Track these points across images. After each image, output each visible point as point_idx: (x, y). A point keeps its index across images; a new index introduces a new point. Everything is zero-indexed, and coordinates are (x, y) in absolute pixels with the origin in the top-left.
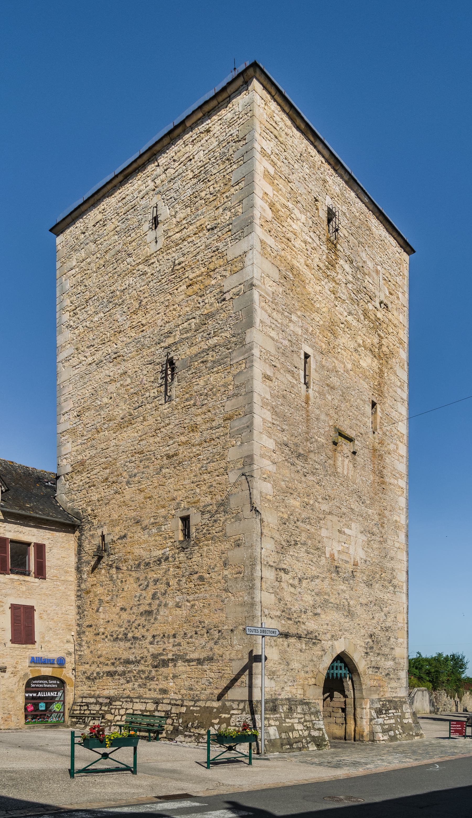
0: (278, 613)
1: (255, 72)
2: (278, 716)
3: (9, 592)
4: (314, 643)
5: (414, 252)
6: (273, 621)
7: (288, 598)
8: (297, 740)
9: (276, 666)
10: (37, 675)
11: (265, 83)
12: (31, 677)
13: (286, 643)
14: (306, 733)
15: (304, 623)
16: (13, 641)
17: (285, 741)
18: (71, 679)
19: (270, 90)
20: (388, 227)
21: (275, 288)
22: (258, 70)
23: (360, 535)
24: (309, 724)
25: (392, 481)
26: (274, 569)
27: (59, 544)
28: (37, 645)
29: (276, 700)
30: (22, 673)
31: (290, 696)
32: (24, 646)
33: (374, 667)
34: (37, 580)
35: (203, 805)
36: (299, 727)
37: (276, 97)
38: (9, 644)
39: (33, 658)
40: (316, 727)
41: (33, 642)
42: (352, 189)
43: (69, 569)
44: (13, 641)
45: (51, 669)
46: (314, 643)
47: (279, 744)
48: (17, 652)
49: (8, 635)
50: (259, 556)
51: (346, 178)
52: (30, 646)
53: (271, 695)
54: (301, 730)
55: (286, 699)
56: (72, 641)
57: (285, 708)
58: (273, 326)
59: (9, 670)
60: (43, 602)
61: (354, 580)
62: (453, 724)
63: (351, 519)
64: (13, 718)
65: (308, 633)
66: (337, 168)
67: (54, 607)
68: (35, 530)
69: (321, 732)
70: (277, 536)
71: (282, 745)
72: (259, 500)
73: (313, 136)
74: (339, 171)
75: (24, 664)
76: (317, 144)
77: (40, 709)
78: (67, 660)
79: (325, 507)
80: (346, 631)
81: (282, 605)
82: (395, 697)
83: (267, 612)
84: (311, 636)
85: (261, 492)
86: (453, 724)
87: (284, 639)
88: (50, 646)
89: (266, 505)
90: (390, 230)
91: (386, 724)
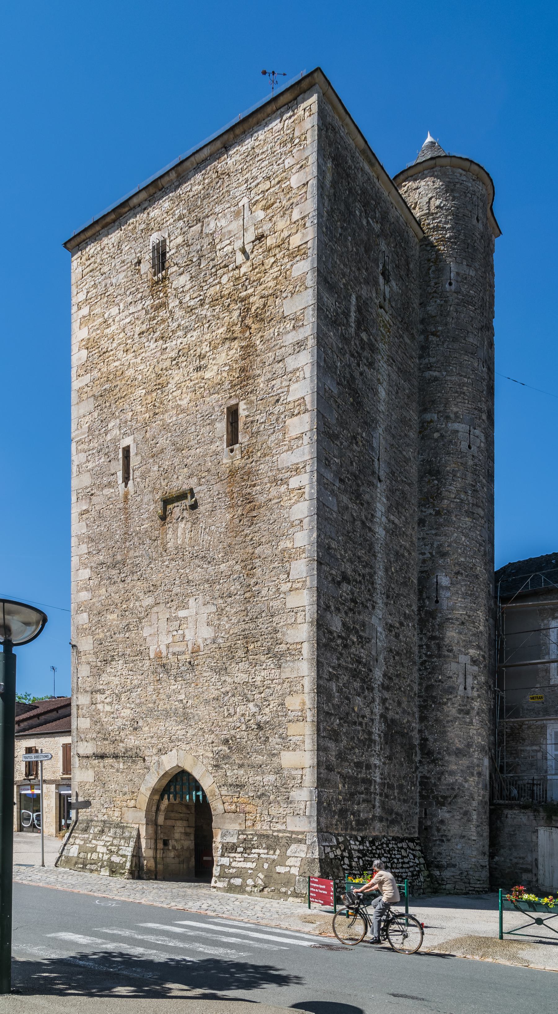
0: (94, 735)
2: (86, 836)
8: (93, 862)
13: (102, 764)
14: (106, 857)
15: (122, 741)
17: (81, 860)
24: (113, 849)
29: (92, 821)
33: (231, 785)
35: (141, 925)
36: (101, 849)
40: (121, 852)
46: (134, 762)
47: (74, 862)
54: (103, 853)
55: (101, 821)
57: (96, 830)
62: (314, 882)
65: (127, 751)
69: (124, 859)
71: (76, 863)
80: (180, 740)
81: (98, 727)
82: (279, 831)
83: (83, 736)
84: (130, 753)
86: (314, 882)
87: (100, 760)
91: (233, 868)
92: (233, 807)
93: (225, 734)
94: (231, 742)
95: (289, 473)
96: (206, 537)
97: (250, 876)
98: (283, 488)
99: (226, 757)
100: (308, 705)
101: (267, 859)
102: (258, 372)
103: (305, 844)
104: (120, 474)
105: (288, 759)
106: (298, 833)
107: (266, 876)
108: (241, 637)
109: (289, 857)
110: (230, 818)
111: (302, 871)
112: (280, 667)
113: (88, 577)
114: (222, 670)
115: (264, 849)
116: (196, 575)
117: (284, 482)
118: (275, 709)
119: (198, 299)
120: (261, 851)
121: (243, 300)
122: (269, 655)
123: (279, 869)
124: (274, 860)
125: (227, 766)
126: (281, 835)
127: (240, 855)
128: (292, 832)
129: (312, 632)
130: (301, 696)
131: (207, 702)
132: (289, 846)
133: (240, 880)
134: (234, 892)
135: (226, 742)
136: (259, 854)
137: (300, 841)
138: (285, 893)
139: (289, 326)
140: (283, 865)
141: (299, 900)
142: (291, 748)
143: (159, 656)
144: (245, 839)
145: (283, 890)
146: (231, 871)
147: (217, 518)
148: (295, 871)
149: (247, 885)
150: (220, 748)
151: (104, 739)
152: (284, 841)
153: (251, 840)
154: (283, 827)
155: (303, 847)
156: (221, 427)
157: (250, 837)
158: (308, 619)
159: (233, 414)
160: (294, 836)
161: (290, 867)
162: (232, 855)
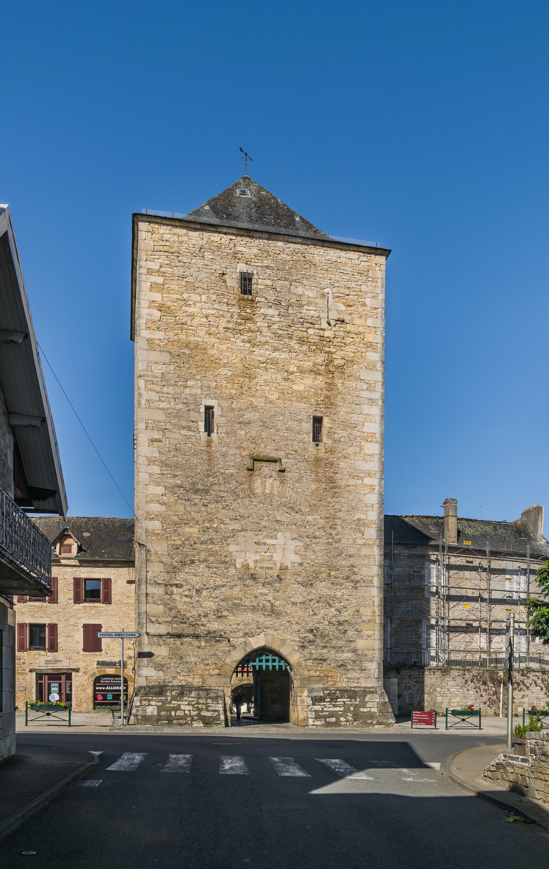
1: (137, 218)
3: (82, 615)
4: (218, 641)
5: (390, 251)
6: (161, 626)
7: (180, 606)
9: (165, 660)
10: (103, 674)
11: (149, 220)
12: (98, 675)
16: (84, 650)
18: (132, 677)
19: (156, 221)
20: (340, 247)
21: (164, 368)
22: (138, 216)
23: (291, 542)
25: (352, 482)
26: (162, 586)
27: (122, 577)
28: (103, 652)
29: (166, 686)
30: (91, 672)
31: (184, 684)
32: (93, 653)
33: (315, 659)
34: (104, 605)
37: (163, 222)
38: (82, 652)
39: (98, 662)
41: (101, 650)
42: (277, 240)
43: (130, 595)
44: (84, 650)
45: (114, 669)
48: (88, 658)
49: (81, 646)
50: (144, 578)
51: (266, 236)
52: (97, 653)
53: (159, 682)
56: (133, 648)
58: (163, 399)
59: (82, 670)
60: (109, 621)
61: (280, 583)
63: (275, 530)
64: (84, 704)
66: (251, 235)
67: (118, 624)
68: (103, 569)
70: (167, 560)
72: (145, 536)
73: (212, 227)
74: (255, 235)
75: (93, 666)
76: (219, 230)
77: (108, 698)
78: (129, 662)
79: (236, 526)
81: (173, 613)
85: (147, 530)
88: (114, 652)
89: (153, 538)
90: (344, 247)
92: (318, 673)
93: (311, 626)
94: (315, 631)
95: (364, 474)
96: (294, 494)
97: (342, 715)
98: (359, 482)
99: (311, 642)
100: (377, 613)
101: (351, 704)
102: (340, 404)
103: (377, 694)
104: (202, 425)
105: (360, 644)
106: (370, 688)
107: (353, 715)
108: (324, 566)
109: (368, 702)
110: (316, 680)
111: (379, 710)
112: (356, 588)
113: (161, 493)
114: (308, 584)
115: (347, 698)
116: (284, 518)
117: (362, 479)
118: (352, 613)
119: (286, 332)
120: (345, 700)
121: (328, 353)
122: (348, 580)
123: (362, 710)
124: (357, 705)
125: (313, 647)
126: (357, 689)
127: (329, 703)
128: (366, 687)
129: (380, 572)
130: (372, 608)
131: (293, 603)
132: (366, 696)
133: (334, 719)
134: (331, 726)
135: (311, 631)
136: (344, 702)
137: (373, 692)
138: (372, 723)
139: (365, 386)
140: (364, 707)
141: (383, 726)
142: (364, 638)
143: (247, 567)
144: (329, 693)
145: (370, 721)
146: (324, 713)
147: (303, 485)
148: (375, 710)
149: (341, 721)
150: (305, 635)
151: (182, 623)
152: (360, 693)
153: (335, 693)
154: (359, 685)
155: (377, 696)
156: (308, 426)
157: (333, 692)
158: (377, 563)
159: (318, 421)
160: (367, 690)
161: (370, 708)
162: (323, 704)
